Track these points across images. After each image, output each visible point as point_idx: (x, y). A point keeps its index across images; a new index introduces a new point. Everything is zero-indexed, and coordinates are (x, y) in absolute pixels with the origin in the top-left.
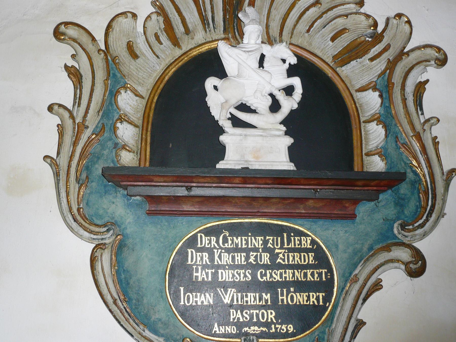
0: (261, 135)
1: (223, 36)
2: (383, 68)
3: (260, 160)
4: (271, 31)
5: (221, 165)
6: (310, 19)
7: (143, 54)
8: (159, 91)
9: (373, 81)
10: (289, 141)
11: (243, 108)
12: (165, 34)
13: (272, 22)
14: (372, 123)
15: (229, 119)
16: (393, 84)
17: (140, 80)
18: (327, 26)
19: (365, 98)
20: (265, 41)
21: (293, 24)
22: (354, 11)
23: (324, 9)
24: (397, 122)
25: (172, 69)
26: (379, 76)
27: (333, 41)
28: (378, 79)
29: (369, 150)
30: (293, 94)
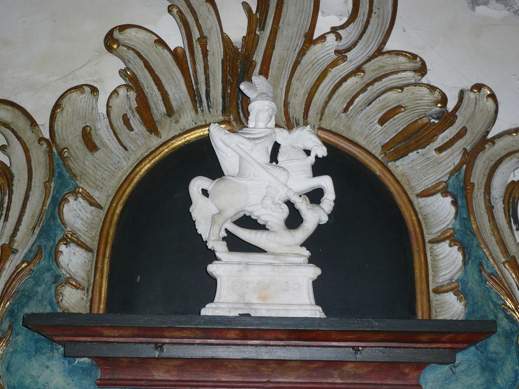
0: (271, 264)
1: (221, 118)
2: (457, 162)
4: (291, 111)
6: (348, 93)
9: (443, 182)
10: (314, 272)
11: (247, 222)
12: (138, 116)
14: (443, 244)
15: (224, 239)
16: (473, 185)
17: (97, 182)
18: (373, 103)
19: (432, 206)
21: (323, 101)
22: (413, 81)
24: (481, 242)
26: (452, 173)
28: (449, 178)
29: (439, 285)
30: (321, 200)
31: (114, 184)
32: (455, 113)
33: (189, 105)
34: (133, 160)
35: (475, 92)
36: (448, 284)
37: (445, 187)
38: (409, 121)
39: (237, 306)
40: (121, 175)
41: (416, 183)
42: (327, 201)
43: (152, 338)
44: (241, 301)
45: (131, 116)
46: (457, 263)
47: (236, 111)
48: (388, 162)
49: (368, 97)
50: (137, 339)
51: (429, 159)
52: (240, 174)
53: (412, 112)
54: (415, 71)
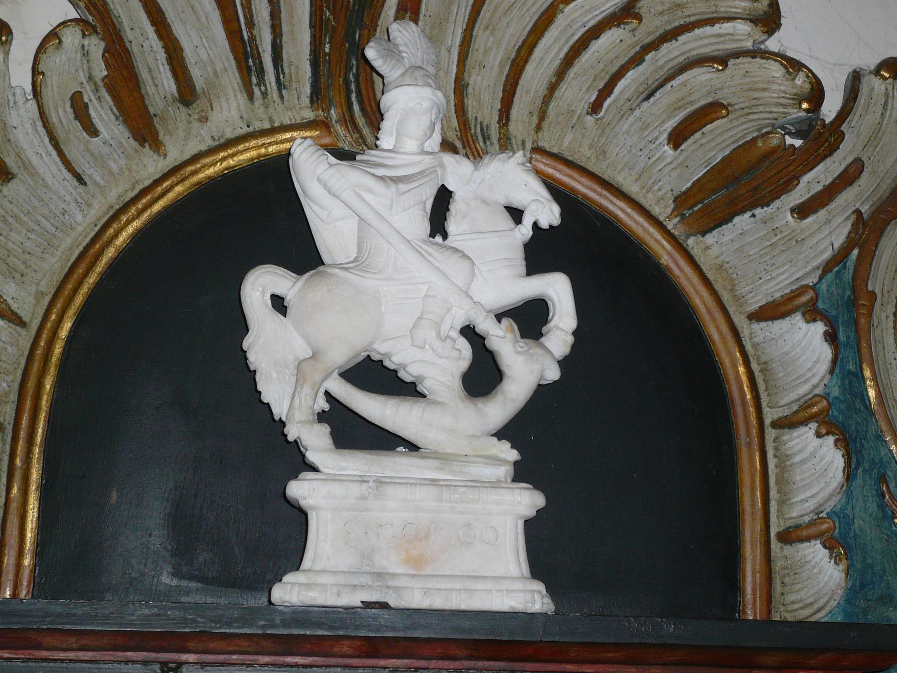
0: (434, 482)
1: (309, 114)
2: (839, 240)
3: (428, 571)
4: (471, 103)
5: (289, 592)
6: (601, 66)
7: (27, 166)
8: (79, 300)
9: (807, 287)
10: (528, 501)
11: (374, 374)
12: (108, 98)
13: (474, 73)
14: (803, 430)
15: (322, 417)
16: (872, 296)
17: (12, 260)
18: (657, 95)
19: (781, 342)
20: (453, 137)
21: (545, 84)
22: (748, 44)
23: (649, 34)
24: (884, 427)
25: (129, 222)
26: (827, 268)
27: (676, 147)
28: (821, 278)
29: (790, 523)
30: (544, 329)
31: (54, 265)
32: (841, 126)
33: (232, 79)
34: (98, 210)
35: (885, 79)
36: (812, 523)
37: (812, 298)
38: (737, 141)
39: (355, 582)
40: (69, 245)
41: (749, 288)
42: (559, 333)
43: (158, 652)
44: (365, 569)
45: (93, 98)
46: (831, 475)
47: (350, 109)
48: (688, 237)
49: (647, 79)
50: (121, 654)
51: (778, 232)
52: (359, 264)
53: (742, 120)
54: (754, 21)
